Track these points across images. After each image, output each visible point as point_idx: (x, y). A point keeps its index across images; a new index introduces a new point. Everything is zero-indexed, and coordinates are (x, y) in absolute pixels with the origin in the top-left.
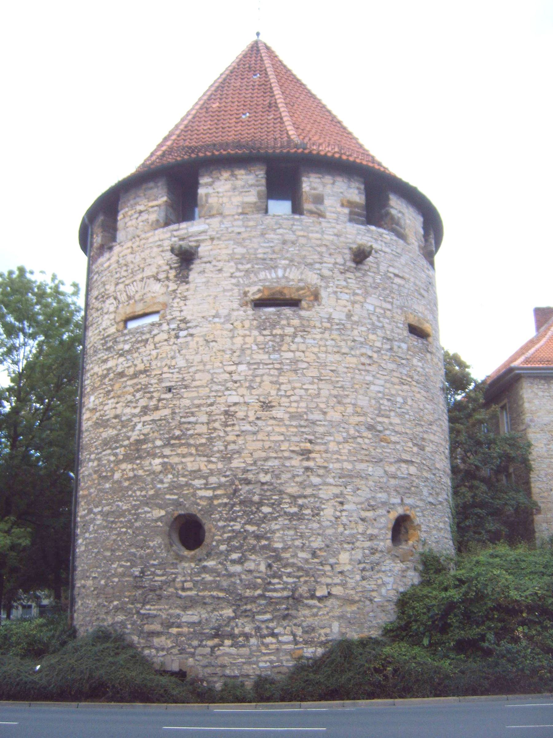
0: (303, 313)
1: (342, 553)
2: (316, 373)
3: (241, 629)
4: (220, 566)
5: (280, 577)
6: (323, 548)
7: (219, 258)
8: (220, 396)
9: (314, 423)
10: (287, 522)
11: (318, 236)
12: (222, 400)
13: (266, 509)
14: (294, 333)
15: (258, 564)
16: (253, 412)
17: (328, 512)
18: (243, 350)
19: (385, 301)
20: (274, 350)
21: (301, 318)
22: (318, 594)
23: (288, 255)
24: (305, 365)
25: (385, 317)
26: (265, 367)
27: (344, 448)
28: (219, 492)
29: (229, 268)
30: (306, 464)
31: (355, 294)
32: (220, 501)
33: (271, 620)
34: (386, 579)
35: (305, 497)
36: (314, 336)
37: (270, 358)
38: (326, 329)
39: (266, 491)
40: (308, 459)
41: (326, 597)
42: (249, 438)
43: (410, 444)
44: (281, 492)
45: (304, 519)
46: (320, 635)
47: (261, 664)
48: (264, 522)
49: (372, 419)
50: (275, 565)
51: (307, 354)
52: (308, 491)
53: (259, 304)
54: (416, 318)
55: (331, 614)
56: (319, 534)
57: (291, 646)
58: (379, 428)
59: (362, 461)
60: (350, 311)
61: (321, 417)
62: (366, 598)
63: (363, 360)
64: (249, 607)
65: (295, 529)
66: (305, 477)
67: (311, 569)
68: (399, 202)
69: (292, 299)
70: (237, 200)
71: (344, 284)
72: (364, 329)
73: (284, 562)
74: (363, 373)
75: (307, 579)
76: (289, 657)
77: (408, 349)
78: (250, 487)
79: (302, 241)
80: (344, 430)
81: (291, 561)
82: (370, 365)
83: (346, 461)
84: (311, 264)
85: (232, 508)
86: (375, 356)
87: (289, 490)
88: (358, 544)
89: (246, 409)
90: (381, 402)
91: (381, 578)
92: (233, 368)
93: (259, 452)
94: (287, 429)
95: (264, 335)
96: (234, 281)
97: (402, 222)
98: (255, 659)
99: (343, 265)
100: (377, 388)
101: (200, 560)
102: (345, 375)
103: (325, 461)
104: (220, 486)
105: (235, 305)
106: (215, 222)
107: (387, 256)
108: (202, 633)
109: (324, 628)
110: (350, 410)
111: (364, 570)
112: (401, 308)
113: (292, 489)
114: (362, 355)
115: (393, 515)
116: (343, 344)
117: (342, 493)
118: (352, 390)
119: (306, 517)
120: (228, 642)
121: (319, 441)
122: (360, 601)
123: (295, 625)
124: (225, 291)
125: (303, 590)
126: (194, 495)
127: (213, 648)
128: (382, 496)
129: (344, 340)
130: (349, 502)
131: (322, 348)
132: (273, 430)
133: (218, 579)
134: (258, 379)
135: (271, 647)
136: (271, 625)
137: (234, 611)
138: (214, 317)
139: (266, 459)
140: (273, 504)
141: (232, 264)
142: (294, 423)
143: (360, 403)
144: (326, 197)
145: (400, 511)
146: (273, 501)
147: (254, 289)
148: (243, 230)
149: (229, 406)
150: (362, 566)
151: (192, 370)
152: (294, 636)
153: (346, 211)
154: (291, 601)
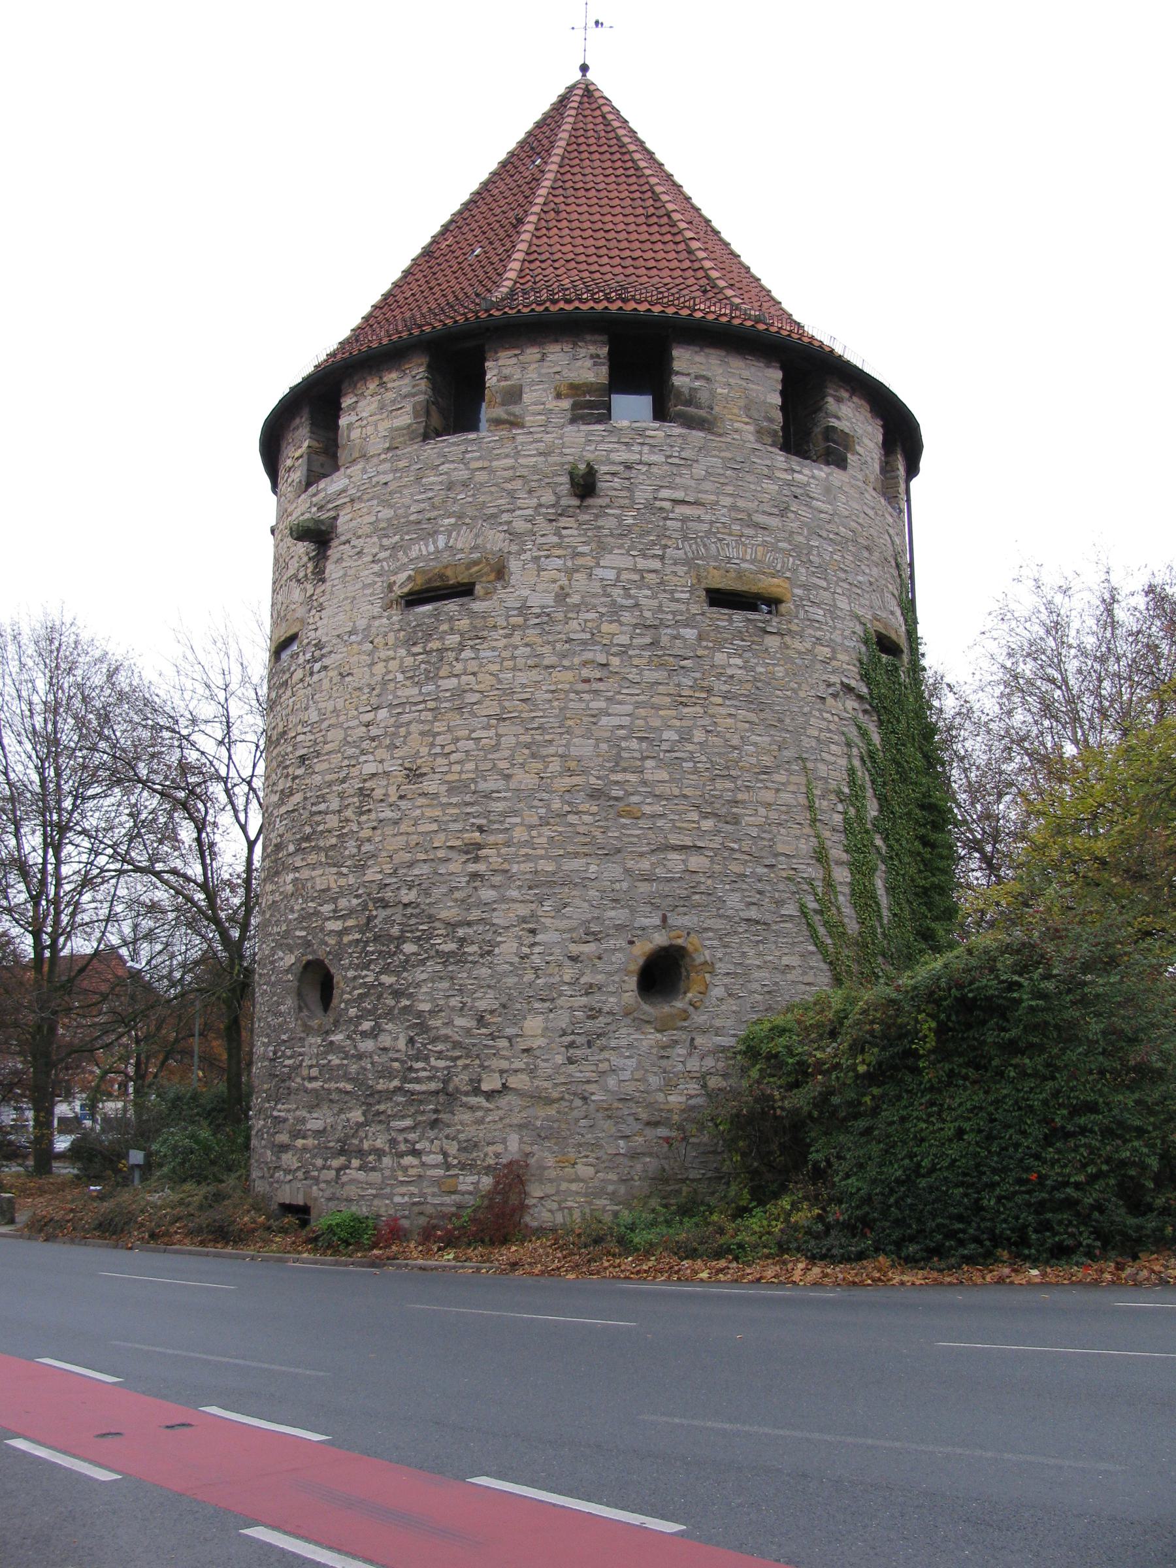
0: (477, 606)
1: (529, 1017)
2: (495, 709)
3: (371, 1142)
4: (348, 1042)
5: (426, 1059)
6: (494, 1011)
7: (360, 532)
8: (354, 766)
9: (488, 796)
10: (439, 967)
11: (509, 462)
12: (354, 772)
13: (409, 948)
14: (460, 643)
15: (395, 1036)
16: (395, 787)
17: (508, 948)
18: (384, 683)
19: (644, 556)
20: (428, 678)
21: (472, 614)
22: (485, 1087)
23: (456, 508)
24: (475, 697)
25: (641, 584)
26: (414, 708)
27: (540, 835)
28: (350, 923)
29: (371, 546)
30: (472, 867)
31: (576, 555)
32: (351, 937)
33: (413, 1129)
34: (616, 1061)
35: (469, 924)
36: (494, 644)
37: (421, 693)
38: (514, 627)
39: (409, 918)
40: (477, 859)
41: (500, 1092)
42: (389, 830)
43: (695, 816)
44: (431, 918)
45: (466, 962)
46: (486, 1155)
47: (397, 1199)
48: (405, 970)
49: (598, 778)
50: (419, 1039)
51: (480, 677)
52: (475, 914)
53: (414, 599)
54: (733, 575)
55: (507, 1121)
56: (489, 987)
57: (440, 1172)
58: (617, 792)
59: (576, 855)
60: (562, 588)
61: (501, 784)
62: (575, 1094)
63: (585, 673)
64: (382, 1107)
65: (452, 978)
66: (470, 890)
67: (474, 1045)
68: (699, 358)
69: (460, 584)
70: (384, 427)
71: (555, 539)
72: (592, 615)
73: (433, 1033)
74: (586, 696)
75: (468, 1062)
76: (436, 1190)
77: (700, 638)
78: (389, 911)
79: (481, 477)
80: (540, 804)
81: (443, 1032)
82: (600, 680)
83: (542, 857)
84: (494, 516)
85: (365, 947)
86: (615, 661)
87: (444, 914)
88: (561, 1001)
89: (385, 783)
90: (623, 744)
91: (608, 1060)
92: (370, 716)
93: (401, 853)
94: (443, 811)
95: (415, 655)
96: (376, 568)
97: (703, 396)
98: (388, 1190)
99: (553, 506)
100: (616, 721)
101: (327, 1033)
102: (547, 706)
103: (505, 860)
104: (351, 912)
105: (377, 610)
106: (356, 470)
107: (654, 470)
108: (327, 1148)
109: (493, 1143)
110: (555, 766)
111: (571, 1045)
112: (688, 562)
113: (449, 912)
114: (585, 664)
115: (642, 949)
116: (547, 649)
117: (533, 915)
118: (559, 730)
119: (470, 958)
120: (355, 1163)
121: (496, 826)
122: (562, 1099)
123: (447, 1137)
124: (365, 586)
125: (461, 1080)
126: (322, 929)
127: (338, 1170)
128: (618, 915)
129: (549, 643)
130: (546, 929)
131: (505, 663)
132: (423, 814)
133: (345, 1062)
134: (403, 731)
135: (411, 1172)
136: (412, 1136)
137: (364, 1114)
138: (350, 633)
139: (411, 865)
140: (419, 938)
141: (375, 539)
142: (454, 800)
143: (574, 752)
144: (526, 389)
145: (660, 939)
146: (419, 934)
147: (402, 577)
148: (390, 477)
149: (365, 781)
150: (568, 1039)
151: (325, 725)
152: (446, 1155)
153: (566, 404)
154: (442, 1098)
